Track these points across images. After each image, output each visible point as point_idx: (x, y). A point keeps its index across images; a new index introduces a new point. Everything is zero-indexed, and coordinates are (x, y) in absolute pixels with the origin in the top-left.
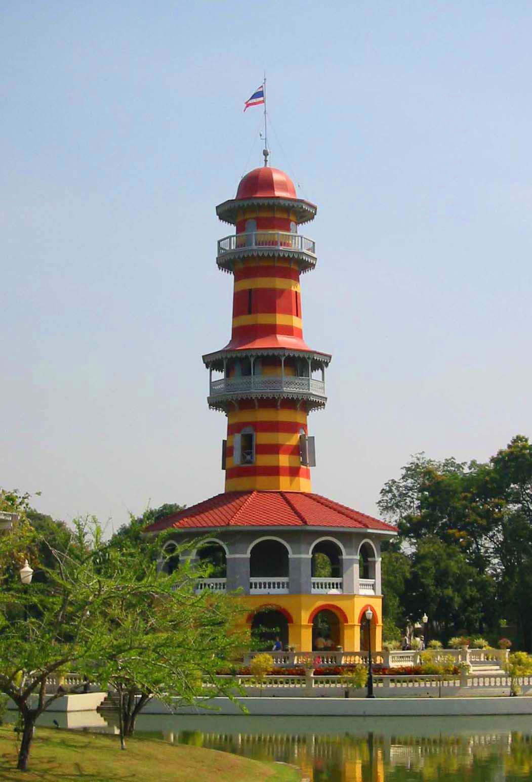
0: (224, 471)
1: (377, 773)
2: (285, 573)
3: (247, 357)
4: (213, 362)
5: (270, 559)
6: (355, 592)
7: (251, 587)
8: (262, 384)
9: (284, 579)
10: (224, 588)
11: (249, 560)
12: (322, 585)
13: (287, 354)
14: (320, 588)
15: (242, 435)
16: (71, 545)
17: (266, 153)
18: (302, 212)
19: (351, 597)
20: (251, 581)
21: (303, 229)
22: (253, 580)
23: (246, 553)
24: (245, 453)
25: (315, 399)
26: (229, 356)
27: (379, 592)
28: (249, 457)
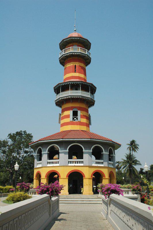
4: (58, 89)
5: (76, 152)
7: (69, 163)
10: (58, 163)
11: (91, 153)
12: (97, 163)
14: (80, 164)
15: (73, 111)
23: (66, 150)
24: (74, 117)
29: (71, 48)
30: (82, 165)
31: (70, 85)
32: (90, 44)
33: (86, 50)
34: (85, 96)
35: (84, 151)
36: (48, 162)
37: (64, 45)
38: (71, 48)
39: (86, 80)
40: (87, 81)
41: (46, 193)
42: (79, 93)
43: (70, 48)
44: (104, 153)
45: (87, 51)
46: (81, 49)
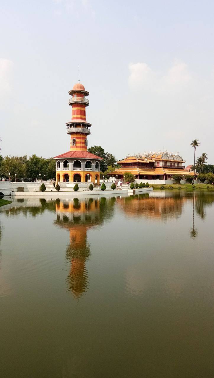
4: (70, 125)
8: (80, 129)
9: (91, 169)
17: (79, 81)
18: (86, 94)
21: (86, 97)
22: (74, 168)
35: (81, 164)
37: (72, 93)
42: (80, 129)
44: (92, 164)
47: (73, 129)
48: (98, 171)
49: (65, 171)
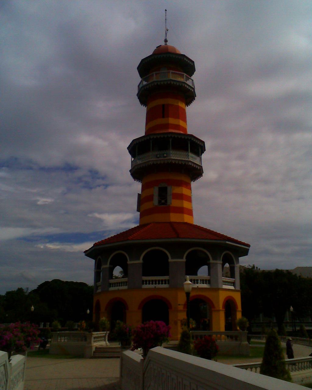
0: (139, 213)
1: (53, 249)
2: (167, 274)
3: (188, 139)
5: (156, 265)
6: (220, 287)
7: (143, 284)
9: (166, 278)
13: (173, 136)
14: (151, 284)
16: (187, 277)
19: (217, 289)
20: (143, 279)
22: (145, 278)
25: (197, 167)
26: (155, 137)
27: (238, 288)
28: (163, 201)
29: (154, 75)
30: (166, 286)
31: (151, 141)
32: (193, 62)
33: (183, 75)
34: (179, 159)
35: (170, 260)
36: (143, 281)
38: (154, 75)
39: (185, 130)
40: (189, 132)
41: (162, 343)
43: (153, 75)
45: (185, 76)
46: (174, 73)
47: (151, 157)
48: (232, 288)
49: (155, 289)
